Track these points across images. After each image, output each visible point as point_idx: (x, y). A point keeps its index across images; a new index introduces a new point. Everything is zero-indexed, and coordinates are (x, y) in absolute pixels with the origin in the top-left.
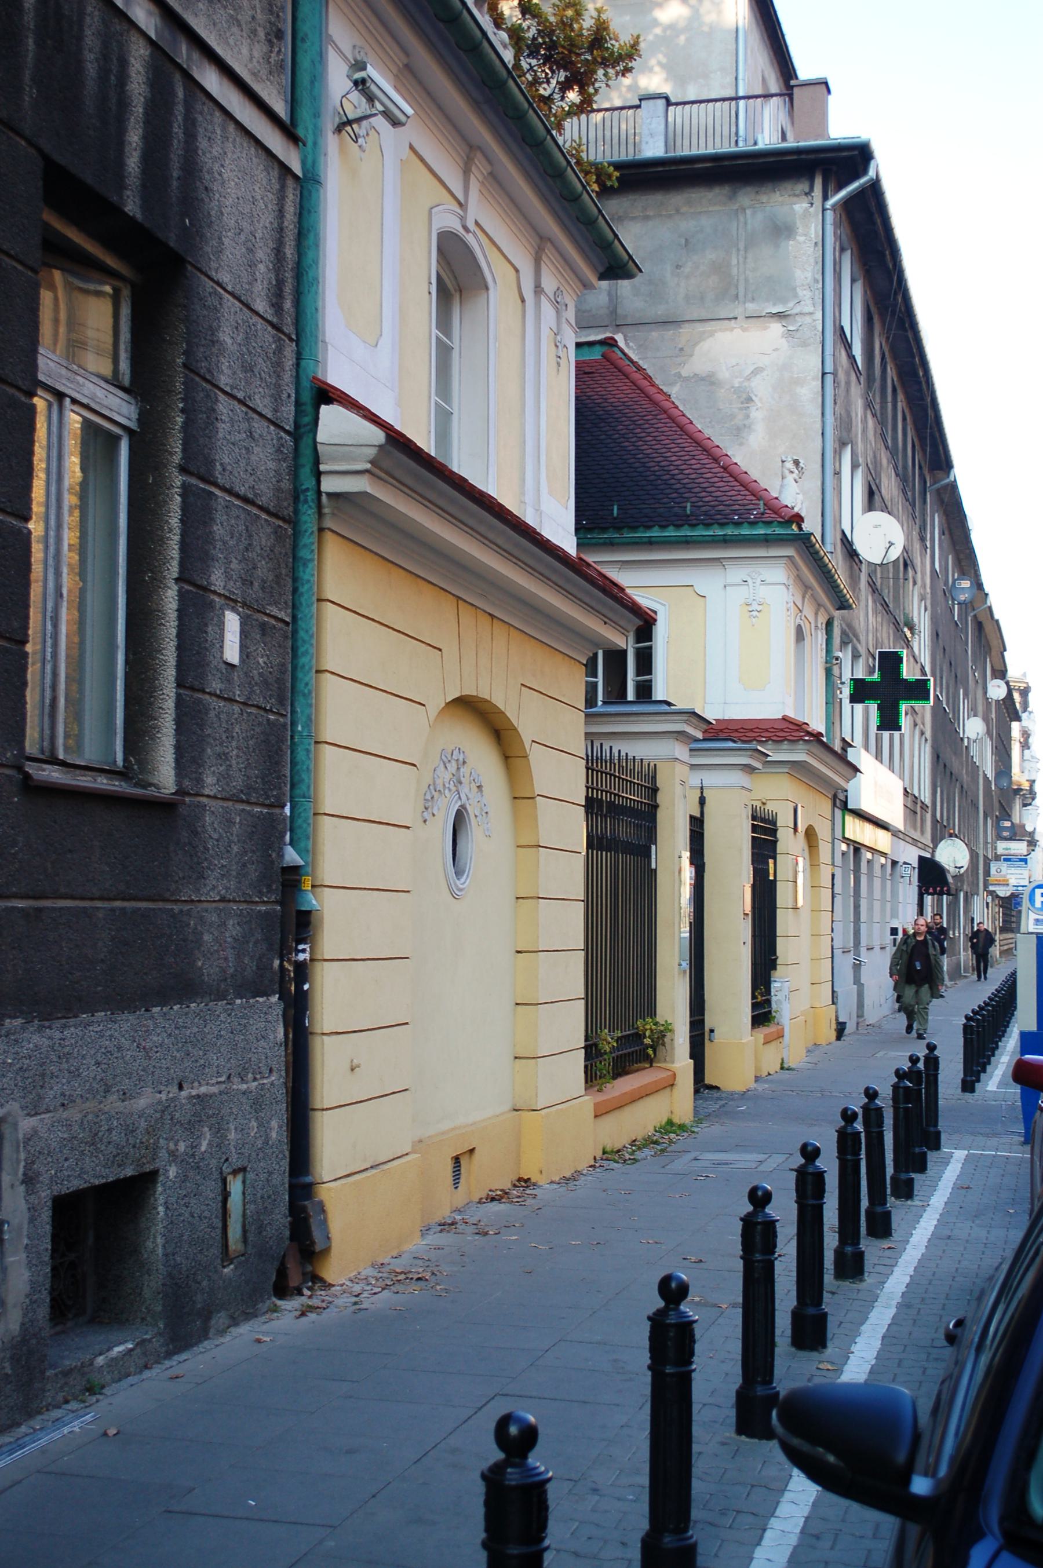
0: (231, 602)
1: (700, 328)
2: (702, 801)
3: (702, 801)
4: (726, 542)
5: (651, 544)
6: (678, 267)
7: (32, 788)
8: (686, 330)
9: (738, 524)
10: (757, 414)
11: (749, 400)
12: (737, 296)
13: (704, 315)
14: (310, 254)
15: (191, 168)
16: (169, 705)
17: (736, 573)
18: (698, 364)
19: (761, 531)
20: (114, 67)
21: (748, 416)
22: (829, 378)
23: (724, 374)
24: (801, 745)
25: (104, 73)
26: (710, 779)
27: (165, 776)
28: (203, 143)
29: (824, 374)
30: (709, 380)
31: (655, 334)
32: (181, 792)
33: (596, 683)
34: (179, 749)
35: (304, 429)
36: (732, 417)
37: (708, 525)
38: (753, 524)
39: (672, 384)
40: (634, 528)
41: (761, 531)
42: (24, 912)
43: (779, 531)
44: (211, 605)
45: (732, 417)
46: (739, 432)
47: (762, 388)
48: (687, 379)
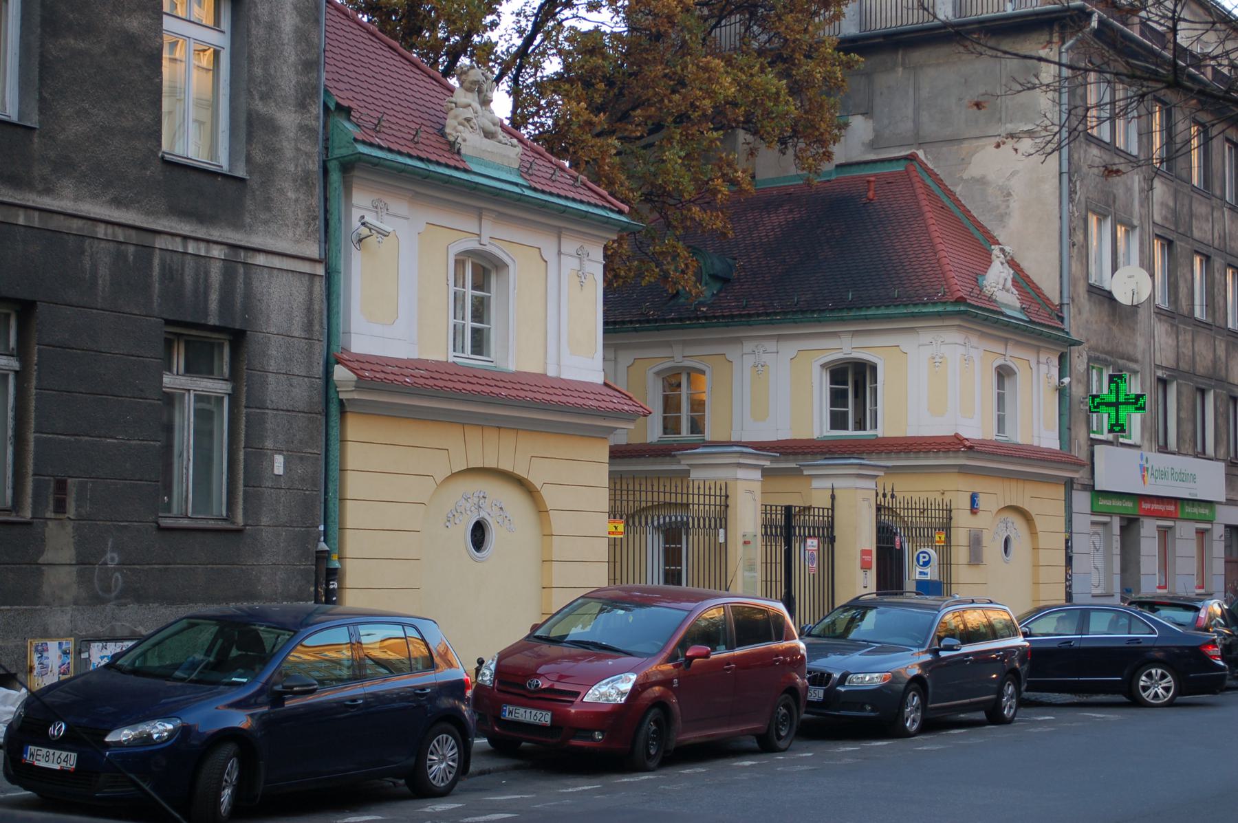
0: (279, 451)
1: (975, 143)
2: (833, 497)
3: (833, 497)
4: (914, 316)
5: (867, 319)
6: (960, 99)
7: (160, 529)
8: (966, 145)
9: (925, 304)
10: (1014, 205)
11: (1009, 194)
12: (1000, 119)
13: (978, 134)
14: (335, 302)
15: (248, 296)
16: (241, 493)
17: (925, 337)
18: (974, 170)
19: (939, 309)
20: (202, 276)
21: (1008, 207)
22: (1065, 177)
23: (991, 177)
24: (961, 454)
25: (196, 281)
26: (838, 483)
27: (240, 519)
28: (256, 283)
29: (1061, 174)
30: (982, 181)
31: (944, 149)
32: (245, 525)
33: (847, 412)
34: (245, 509)
35: (328, 373)
36: (998, 207)
37: (906, 305)
38: (935, 304)
39: (957, 185)
40: (860, 309)
41: (939, 309)
42: (160, 570)
43: (949, 308)
44: (265, 454)
45: (998, 207)
46: (1002, 218)
47: (1017, 185)
48: (967, 181)
